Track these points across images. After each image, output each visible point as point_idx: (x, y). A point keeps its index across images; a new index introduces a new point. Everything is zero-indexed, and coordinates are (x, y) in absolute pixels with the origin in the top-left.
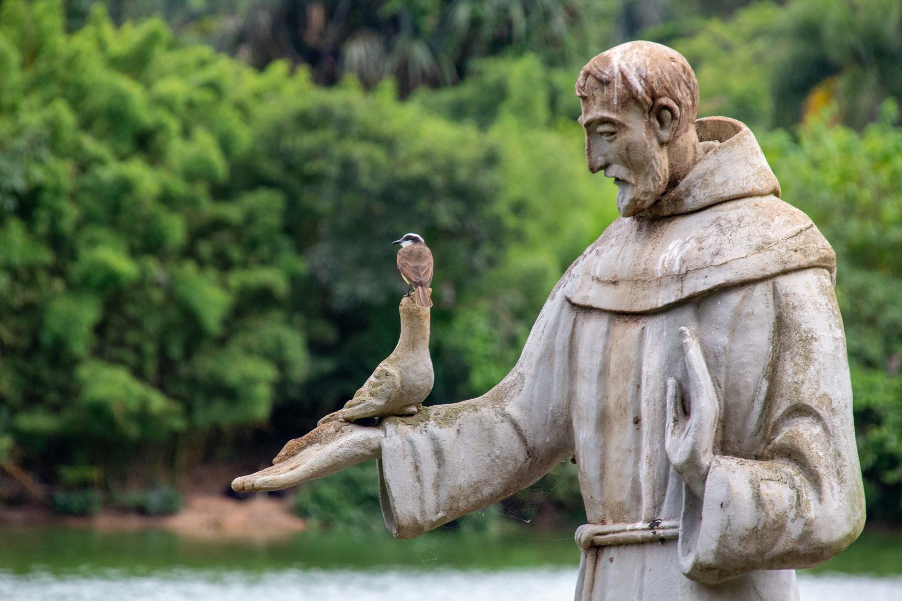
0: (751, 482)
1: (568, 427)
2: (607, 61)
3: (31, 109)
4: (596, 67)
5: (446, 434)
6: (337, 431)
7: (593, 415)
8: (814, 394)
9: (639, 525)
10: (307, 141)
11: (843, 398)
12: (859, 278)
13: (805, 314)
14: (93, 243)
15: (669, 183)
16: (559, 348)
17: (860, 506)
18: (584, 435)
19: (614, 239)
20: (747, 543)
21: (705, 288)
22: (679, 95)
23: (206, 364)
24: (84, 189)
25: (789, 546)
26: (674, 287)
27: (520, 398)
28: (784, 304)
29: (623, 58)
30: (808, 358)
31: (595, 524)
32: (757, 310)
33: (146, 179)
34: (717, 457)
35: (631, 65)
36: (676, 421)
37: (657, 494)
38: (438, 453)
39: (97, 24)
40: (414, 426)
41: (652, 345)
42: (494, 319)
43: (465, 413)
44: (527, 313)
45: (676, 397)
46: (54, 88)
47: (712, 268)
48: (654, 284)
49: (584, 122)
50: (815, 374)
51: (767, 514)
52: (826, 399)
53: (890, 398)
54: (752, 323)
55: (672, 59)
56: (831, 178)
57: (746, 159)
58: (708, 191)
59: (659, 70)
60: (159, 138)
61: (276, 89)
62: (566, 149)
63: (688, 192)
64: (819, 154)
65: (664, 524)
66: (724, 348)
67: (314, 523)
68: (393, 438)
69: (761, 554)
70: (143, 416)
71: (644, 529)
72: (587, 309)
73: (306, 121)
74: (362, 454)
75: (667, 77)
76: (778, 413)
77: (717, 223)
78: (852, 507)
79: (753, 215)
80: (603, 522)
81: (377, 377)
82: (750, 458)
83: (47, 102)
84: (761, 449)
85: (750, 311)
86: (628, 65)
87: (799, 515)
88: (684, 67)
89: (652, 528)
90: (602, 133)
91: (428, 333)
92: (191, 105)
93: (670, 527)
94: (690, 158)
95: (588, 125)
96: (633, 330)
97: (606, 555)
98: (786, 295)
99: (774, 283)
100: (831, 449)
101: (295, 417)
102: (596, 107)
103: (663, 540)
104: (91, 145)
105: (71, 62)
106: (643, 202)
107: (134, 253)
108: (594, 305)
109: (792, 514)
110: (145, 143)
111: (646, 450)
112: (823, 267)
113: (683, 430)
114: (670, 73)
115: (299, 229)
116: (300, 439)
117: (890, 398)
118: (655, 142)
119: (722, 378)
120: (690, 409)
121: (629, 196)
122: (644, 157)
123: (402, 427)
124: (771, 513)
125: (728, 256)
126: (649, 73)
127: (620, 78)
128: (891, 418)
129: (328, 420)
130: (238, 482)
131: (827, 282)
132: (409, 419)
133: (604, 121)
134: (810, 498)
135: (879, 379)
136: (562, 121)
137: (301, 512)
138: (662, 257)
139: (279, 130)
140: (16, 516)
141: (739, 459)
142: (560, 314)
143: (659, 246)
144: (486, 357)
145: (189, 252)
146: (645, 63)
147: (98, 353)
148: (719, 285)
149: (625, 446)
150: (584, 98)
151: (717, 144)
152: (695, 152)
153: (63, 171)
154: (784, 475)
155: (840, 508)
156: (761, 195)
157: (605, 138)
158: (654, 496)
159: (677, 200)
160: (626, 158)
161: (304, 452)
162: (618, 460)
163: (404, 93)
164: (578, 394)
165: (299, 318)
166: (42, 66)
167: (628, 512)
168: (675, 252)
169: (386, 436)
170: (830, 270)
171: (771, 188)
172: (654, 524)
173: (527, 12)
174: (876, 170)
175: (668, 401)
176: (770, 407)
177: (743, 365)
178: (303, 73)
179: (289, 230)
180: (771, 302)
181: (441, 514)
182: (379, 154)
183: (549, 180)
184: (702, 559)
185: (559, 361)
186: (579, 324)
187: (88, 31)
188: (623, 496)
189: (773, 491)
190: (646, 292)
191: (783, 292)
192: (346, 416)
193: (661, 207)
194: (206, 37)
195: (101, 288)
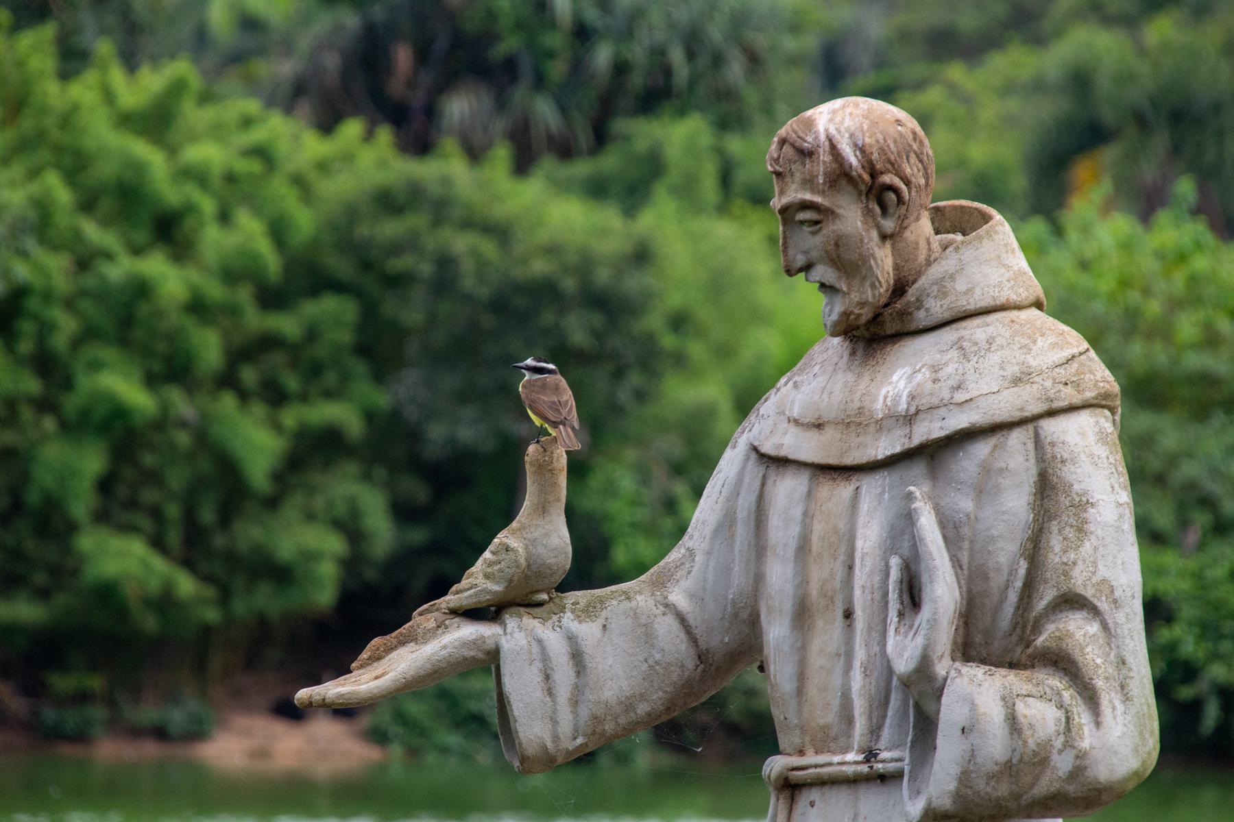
0: (1003, 699)
1: (754, 622)
2: (810, 124)
4: (795, 132)
5: (588, 631)
6: (439, 627)
7: (788, 605)
8: (1090, 579)
9: (851, 757)
10: (390, 229)
11: (1128, 586)
12: (1145, 420)
13: (1079, 470)
14: (96, 366)
15: (894, 291)
17: (1152, 732)
19: (817, 367)
20: (997, 782)
21: (942, 434)
22: (908, 170)
23: (249, 533)
24: (84, 293)
25: (1056, 786)
26: (900, 432)
27: (687, 583)
28: (1049, 456)
29: (831, 120)
30: (1081, 530)
31: (789, 755)
32: (1012, 465)
33: (170, 279)
34: (957, 664)
35: (842, 130)
36: (901, 615)
37: (875, 714)
38: (577, 656)
39: (103, 68)
40: (544, 620)
41: (869, 513)
42: (643, 475)
43: (614, 602)
44: (695, 466)
45: (901, 582)
46: (44, 155)
47: (952, 407)
48: (872, 428)
49: (779, 207)
50: (1090, 551)
51: (1025, 742)
52: (1107, 587)
53: (1185, 585)
54: (1005, 482)
55: (899, 122)
56: (1106, 285)
57: (998, 259)
58: (946, 302)
59: (880, 137)
60: (189, 223)
61: (348, 158)
62: (744, 242)
63: (919, 304)
64: (1089, 252)
65: (884, 755)
66: (968, 516)
67: (396, 750)
68: (515, 636)
69: (1017, 796)
70: (165, 603)
71: (856, 763)
72: (781, 462)
73: (388, 202)
74: (473, 657)
75: (892, 146)
76: (1041, 605)
77: (959, 345)
78: (1141, 733)
79: (1007, 335)
80: (801, 753)
81: (493, 553)
82: (1003, 667)
83: (34, 174)
84: (1017, 653)
85: (1003, 465)
86: (838, 130)
87: (1068, 744)
88: (914, 133)
89: (867, 760)
90: (802, 222)
91: (564, 493)
92: (231, 178)
93: (893, 760)
94: (922, 257)
95: (784, 211)
96: (845, 490)
97: (805, 797)
98: (1053, 444)
99: (1036, 429)
100: (1112, 655)
101: (373, 607)
102: (794, 186)
103: (882, 778)
104: (94, 232)
105: (68, 120)
106: (859, 315)
107: (151, 381)
108: (791, 457)
109: (1058, 743)
110: (169, 230)
111: (860, 655)
112: (1103, 407)
113: (911, 627)
114: (895, 142)
115: (378, 348)
116: (388, 637)
117: (1185, 585)
118: (875, 234)
119: (965, 557)
120: (920, 599)
121: (838, 308)
122: (860, 255)
123: (528, 621)
124: (1030, 741)
126: (867, 140)
127: (827, 149)
128: (1187, 612)
129: (428, 611)
130: (303, 694)
131: (1109, 427)
132: (537, 610)
133: (805, 206)
134: (1083, 721)
135: (1169, 559)
136: (739, 204)
137: (378, 736)
138: (884, 391)
139: (352, 213)
141: (987, 668)
142: (743, 469)
143: (879, 377)
144: (633, 525)
145: (227, 380)
146: (861, 127)
147: (102, 517)
148: (962, 430)
149: (832, 648)
150: (779, 174)
151: (959, 237)
152: (930, 249)
153: (55, 268)
154: (1047, 690)
156: (1019, 307)
157: (806, 229)
158: (870, 718)
159: (904, 314)
160: (835, 256)
161: (394, 655)
162: (822, 668)
163: (523, 165)
164: (768, 579)
165: (380, 472)
166: (27, 124)
167: (835, 739)
168: (902, 384)
169: (505, 634)
170: (1112, 410)
171: (1032, 299)
172: (870, 756)
173: (691, 55)
174: (1167, 274)
175: (891, 587)
176: (1029, 597)
177: (993, 539)
178: (385, 135)
179: (363, 350)
180: (1032, 454)
181: (580, 741)
182: (488, 248)
183: (720, 283)
184: (935, 803)
185: (742, 533)
186: (770, 482)
187: (91, 77)
188: (830, 717)
189: (1033, 712)
190: (861, 439)
191: (1049, 440)
192: (452, 605)
193: (882, 323)
194: (252, 86)
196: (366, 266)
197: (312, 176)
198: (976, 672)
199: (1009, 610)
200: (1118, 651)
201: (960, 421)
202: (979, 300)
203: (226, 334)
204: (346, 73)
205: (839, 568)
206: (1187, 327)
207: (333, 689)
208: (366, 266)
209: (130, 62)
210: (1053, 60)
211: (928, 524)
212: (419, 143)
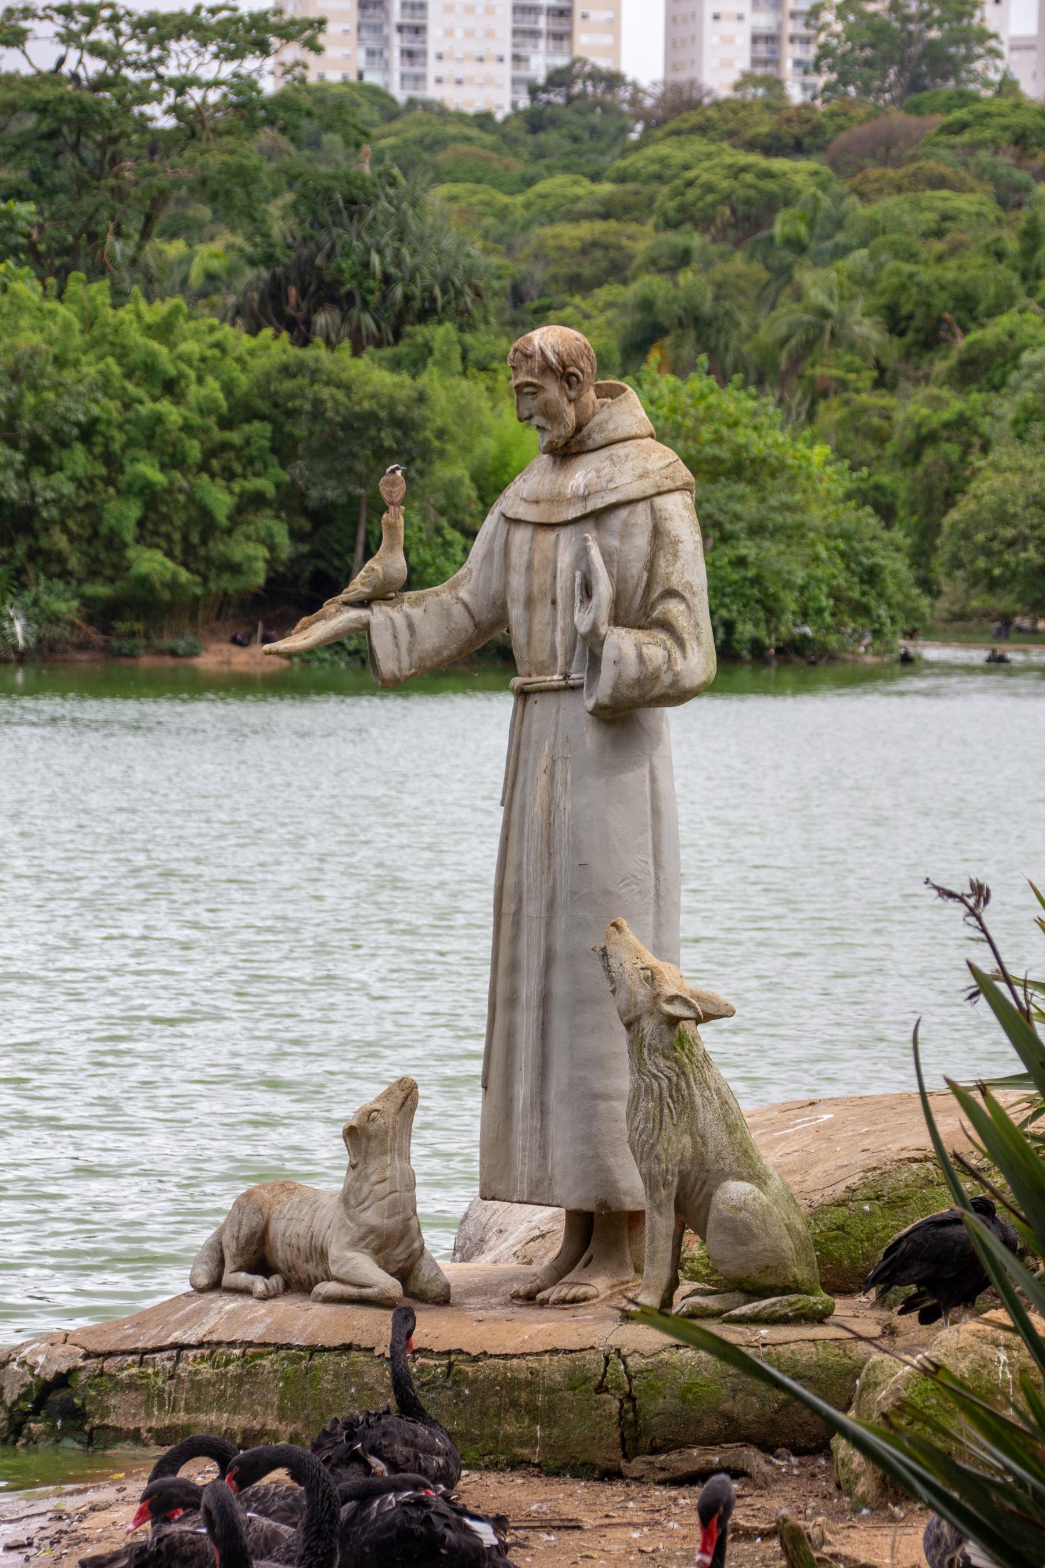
1: (504, 607)
2: (530, 341)
3: (89, 364)
5: (416, 613)
7: (522, 598)
9: (556, 677)
10: (289, 385)
14: (135, 460)
16: (497, 550)
18: (516, 612)
23: (217, 548)
24: (128, 421)
26: (580, 505)
33: (172, 413)
38: (411, 626)
39: (136, 302)
41: (564, 550)
46: (106, 347)
52: (689, 585)
54: (635, 531)
63: (589, 436)
68: (378, 616)
69: (642, 696)
70: (173, 585)
72: (517, 522)
73: (287, 371)
76: (655, 596)
83: (101, 358)
87: (670, 669)
95: (517, 387)
96: (551, 536)
97: (532, 699)
103: (573, 688)
107: (163, 467)
110: (171, 387)
111: (560, 623)
115: (283, 450)
121: (547, 439)
123: (384, 608)
125: (618, 482)
131: (689, 501)
139: (268, 376)
140: (84, 657)
145: (204, 467)
147: (139, 540)
149: (546, 619)
155: (698, 661)
159: (581, 442)
166: (96, 332)
173: (445, 292)
179: (274, 450)
182: (340, 395)
183: (463, 413)
185: (497, 559)
187: (129, 306)
188: (544, 656)
195: (141, 492)
196: (276, 405)
197: (248, 358)
198: (622, 631)
199: (638, 599)
200: (695, 617)
201: (611, 499)
202: (620, 434)
203: (202, 443)
204: (262, 301)
205: (549, 578)
206: (706, 433)
207: (282, 645)
208: (276, 405)
209: (150, 301)
210: (630, 293)
211: (595, 554)
212: (304, 342)
